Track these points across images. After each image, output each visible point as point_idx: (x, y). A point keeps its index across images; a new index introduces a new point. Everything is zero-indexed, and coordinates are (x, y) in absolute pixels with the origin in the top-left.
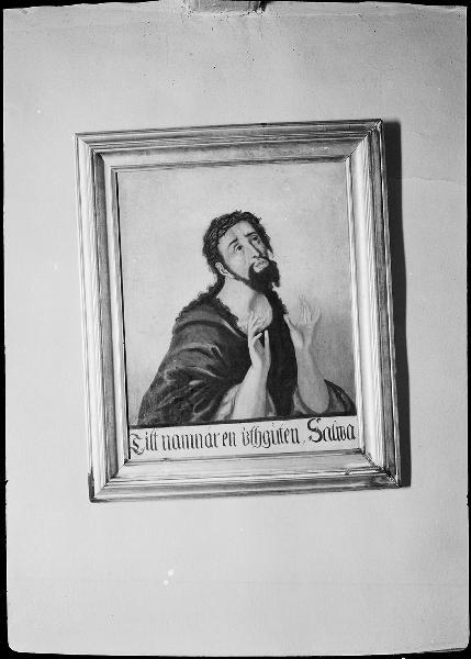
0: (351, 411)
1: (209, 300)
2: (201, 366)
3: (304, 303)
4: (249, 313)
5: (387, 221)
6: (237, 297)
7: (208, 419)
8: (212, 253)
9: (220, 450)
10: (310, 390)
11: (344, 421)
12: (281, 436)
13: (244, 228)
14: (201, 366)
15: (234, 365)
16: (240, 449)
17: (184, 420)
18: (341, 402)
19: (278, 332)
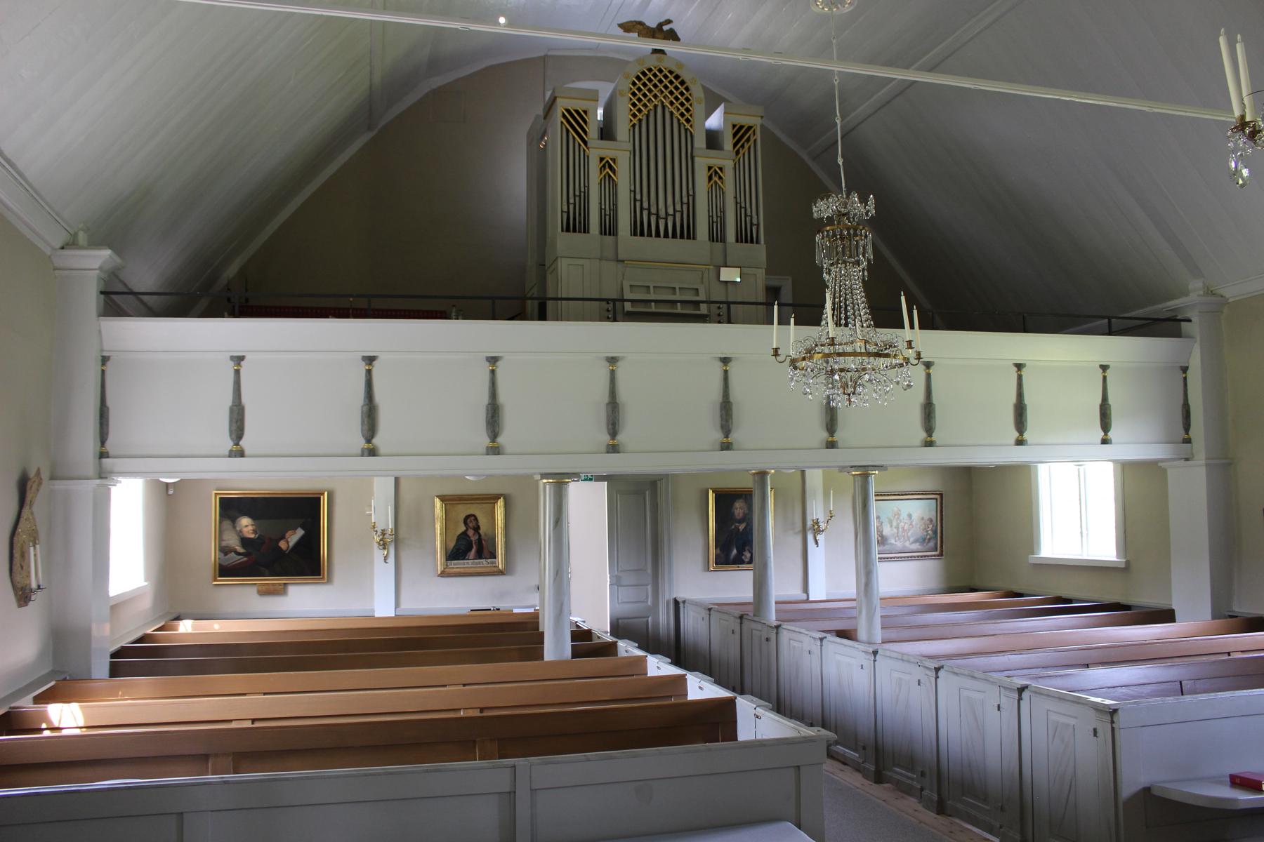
1: (465, 533)
6: (471, 533)
8: (465, 522)
10: (486, 552)
15: (470, 549)
18: (493, 556)
19: (480, 540)
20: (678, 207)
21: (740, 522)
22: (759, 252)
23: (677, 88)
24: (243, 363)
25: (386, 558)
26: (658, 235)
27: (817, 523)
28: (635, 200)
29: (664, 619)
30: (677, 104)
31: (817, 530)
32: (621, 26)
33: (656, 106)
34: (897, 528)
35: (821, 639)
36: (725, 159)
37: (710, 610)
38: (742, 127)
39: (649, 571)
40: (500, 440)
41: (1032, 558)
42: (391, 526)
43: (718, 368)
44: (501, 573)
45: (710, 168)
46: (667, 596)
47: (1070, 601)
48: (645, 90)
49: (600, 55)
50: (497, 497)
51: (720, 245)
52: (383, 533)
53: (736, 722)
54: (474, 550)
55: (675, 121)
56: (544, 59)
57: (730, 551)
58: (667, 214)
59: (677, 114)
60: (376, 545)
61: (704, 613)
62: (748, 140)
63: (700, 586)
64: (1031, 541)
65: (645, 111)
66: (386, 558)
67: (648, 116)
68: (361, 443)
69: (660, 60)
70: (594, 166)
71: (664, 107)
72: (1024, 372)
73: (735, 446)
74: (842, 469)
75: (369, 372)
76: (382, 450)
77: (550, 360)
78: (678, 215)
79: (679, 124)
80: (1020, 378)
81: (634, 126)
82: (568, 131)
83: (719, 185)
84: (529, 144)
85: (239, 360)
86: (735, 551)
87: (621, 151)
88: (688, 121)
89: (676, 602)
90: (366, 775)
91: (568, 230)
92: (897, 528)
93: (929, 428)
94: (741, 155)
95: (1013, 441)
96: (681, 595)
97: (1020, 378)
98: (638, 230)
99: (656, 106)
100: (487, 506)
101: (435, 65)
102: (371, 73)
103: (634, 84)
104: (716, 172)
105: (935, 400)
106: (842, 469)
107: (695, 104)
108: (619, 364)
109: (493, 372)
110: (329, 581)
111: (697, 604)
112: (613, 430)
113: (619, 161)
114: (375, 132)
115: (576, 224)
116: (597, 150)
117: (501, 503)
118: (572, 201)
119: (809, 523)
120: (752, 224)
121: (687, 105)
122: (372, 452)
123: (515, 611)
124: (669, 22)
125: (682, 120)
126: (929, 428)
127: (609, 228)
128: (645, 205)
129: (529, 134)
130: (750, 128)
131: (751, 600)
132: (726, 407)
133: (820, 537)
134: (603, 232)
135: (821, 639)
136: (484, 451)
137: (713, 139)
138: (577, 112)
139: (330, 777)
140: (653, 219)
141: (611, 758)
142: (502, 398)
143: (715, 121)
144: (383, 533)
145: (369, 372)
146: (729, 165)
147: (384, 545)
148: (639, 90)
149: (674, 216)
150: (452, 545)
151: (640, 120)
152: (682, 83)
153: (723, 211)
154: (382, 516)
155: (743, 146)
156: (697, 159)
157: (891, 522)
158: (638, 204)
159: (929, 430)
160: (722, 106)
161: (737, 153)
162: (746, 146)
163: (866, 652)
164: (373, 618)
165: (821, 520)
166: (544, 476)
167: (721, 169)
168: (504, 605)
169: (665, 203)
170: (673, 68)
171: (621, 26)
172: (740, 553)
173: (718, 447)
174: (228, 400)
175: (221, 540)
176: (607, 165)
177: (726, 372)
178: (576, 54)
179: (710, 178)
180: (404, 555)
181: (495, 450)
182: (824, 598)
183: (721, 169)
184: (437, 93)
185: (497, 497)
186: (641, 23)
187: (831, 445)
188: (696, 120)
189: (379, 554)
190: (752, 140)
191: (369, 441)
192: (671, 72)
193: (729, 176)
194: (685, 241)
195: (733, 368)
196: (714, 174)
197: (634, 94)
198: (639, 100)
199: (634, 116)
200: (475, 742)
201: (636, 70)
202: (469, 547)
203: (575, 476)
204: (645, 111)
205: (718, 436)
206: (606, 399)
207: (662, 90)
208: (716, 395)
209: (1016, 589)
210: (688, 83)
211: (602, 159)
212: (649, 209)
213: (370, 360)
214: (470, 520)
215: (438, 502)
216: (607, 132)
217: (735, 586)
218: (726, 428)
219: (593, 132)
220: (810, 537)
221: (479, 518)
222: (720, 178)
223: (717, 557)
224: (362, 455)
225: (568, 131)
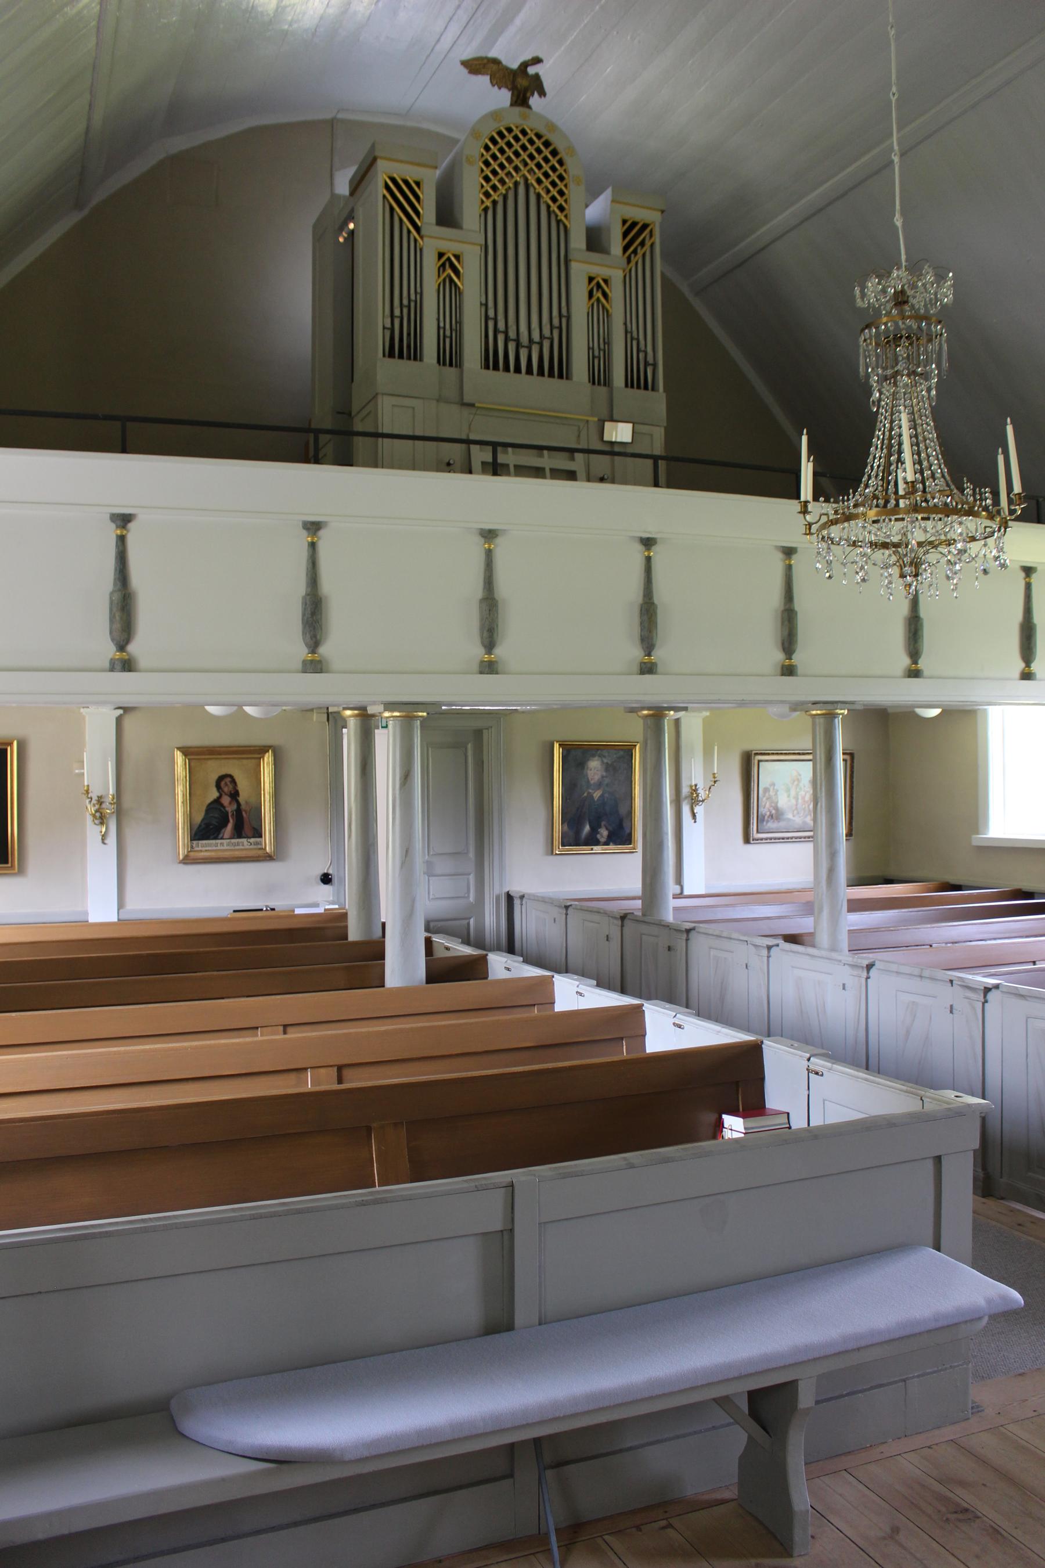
0: (261, 836)
1: (217, 801)
2: (214, 822)
3: (247, 803)
4: (231, 808)
6: (226, 800)
7: (216, 838)
8: (218, 786)
9: (219, 848)
10: (247, 828)
11: (258, 840)
12: (238, 844)
13: (228, 780)
14: (214, 822)
16: (225, 847)
17: (208, 838)
18: (258, 833)
19: (239, 811)
20: (546, 332)
22: (657, 402)
23: (546, 160)
25: (104, 838)
27: (696, 790)
28: (487, 318)
29: (492, 921)
30: (546, 183)
31: (694, 800)
32: (464, 63)
33: (516, 184)
34: (796, 798)
35: (769, 948)
36: (611, 267)
37: (567, 907)
38: (634, 224)
39: (472, 855)
40: (324, 650)
41: (977, 839)
42: (112, 791)
43: (636, 555)
44: (269, 858)
45: (591, 279)
46: (495, 890)
47: (1030, 895)
48: (502, 159)
49: (410, 124)
50: (262, 750)
51: (603, 390)
52: (100, 801)
53: (763, 1079)
54: (230, 826)
55: (543, 208)
56: (332, 123)
58: (531, 340)
59: (546, 198)
60: (89, 819)
61: (558, 913)
62: (642, 244)
63: (543, 874)
64: (974, 812)
65: (502, 190)
66: (104, 838)
67: (505, 198)
68: (110, 650)
69: (525, 117)
71: (527, 186)
72: (1034, 579)
73: (660, 668)
74: (797, 706)
75: (122, 540)
76: (143, 662)
77: (397, 528)
78: (546, 344)
79: (549, 212)
80: (1028, 587)
81: (486, 210)
82: (392, 209)
83: (604, 304)
84: (319, 237)
86: (587, 828)
87: (468, 243)
88: (561, 208)
89: (510, 898)
90: (254, 1218)
91: (391, 355)
92: (796, 798)
93: (914, 651)
94: (633, 264)
95: (1017, 675)
96: (516, 887)
97: (1028, 587)
98: (491, 361)
99: (516, 184)
100: (250, 763)
101: (176, 114)
102: (91, 105)
103: (487, 148)
104: (598, 285)
105: (922, 613)
106: (797, 706)
107: (572, 186)
108: (499, 540)
109: (313, 545)
110: (21, 871)
111: (544, 900)
113: (466, 258)
114: (86, 212)
115: (403, 347)
116: (435, 240)
117: (268, 758)
118: (397, 312)
119: (685, 791)
120: (646, 364)
121: (561, 185)
122: (128, 665)
123: (298, 911)
124: (537, 61)
125: (554, 207)
126: (914, 651)
127: (450, 356)
128: (501, 325)
129: (315, 227)
130: (645, 226)
131: (639, 893)
132: (648, 612)
133: (699, 810)
134: (440, 361)
135: (769, 948)
136: (300, 666)
137: (595, 240)
138: (406, 182)
139: (186, 1226)
140: (512, 347)
141: (667, 1160)
142: (328, 586)
143: (597, 210)
145: (122, 540)
146: (617, 276)
147: (101, 818)
148: (494, 157)
149: (541, 344)
150: (199, 818)
151: (495, 203)
152: (554, 153)
153: (608, 342)
154: (97, 773)
155: (635, 252)
156: (574, 266)
157: (788, 790)
158: (491, 324)
159: (915, 654)
160: (608, 193)
161: (629, 260)
162: (640, 252)
163: (854, 966)
165: (700, 786)
166: (389, 706)
167: (606, 281)
168: (280, 902)
169: (528, 325)
170: (543, 131)
171: (464, 63)
172: (594, 830)
173: (636, 668)
176: (448, 264)
177: (648, 559)
178: (377, 120)
179: (591, 295)
180: (129, 832)
181: (315, 666)
182: (702, 892)
183: (606, 281)
184: (176, 161)
185: (262, 750)
186: (496, 62)
187: (789, 671)
188: (573, 208)
189: (93, 831)
190: (648, 244)
191: (122, 647)
192: (539, 136)
193: (616, 292)
194: (555, 381)
196: (597, 287)
197: (487, 164)
198: (494, 172)
199: (487, 195)
200: (369, 1129)
201: (490, 129)
202: (224, 821)
204: (502, 190)
206: (479, 593)
208: (634, 592)
209: (953, 879)
210: (562, 154)
211: (441, 255)
212: (506, 333)
213: (124, 520)
215: (179, 757)
216: (447, 217)
217: (612, 875)
218: (648, 642)
219: (428, 210)
220: (686, 809)
222: (605, 295)
224: (112, 669)
225: (392, 209)
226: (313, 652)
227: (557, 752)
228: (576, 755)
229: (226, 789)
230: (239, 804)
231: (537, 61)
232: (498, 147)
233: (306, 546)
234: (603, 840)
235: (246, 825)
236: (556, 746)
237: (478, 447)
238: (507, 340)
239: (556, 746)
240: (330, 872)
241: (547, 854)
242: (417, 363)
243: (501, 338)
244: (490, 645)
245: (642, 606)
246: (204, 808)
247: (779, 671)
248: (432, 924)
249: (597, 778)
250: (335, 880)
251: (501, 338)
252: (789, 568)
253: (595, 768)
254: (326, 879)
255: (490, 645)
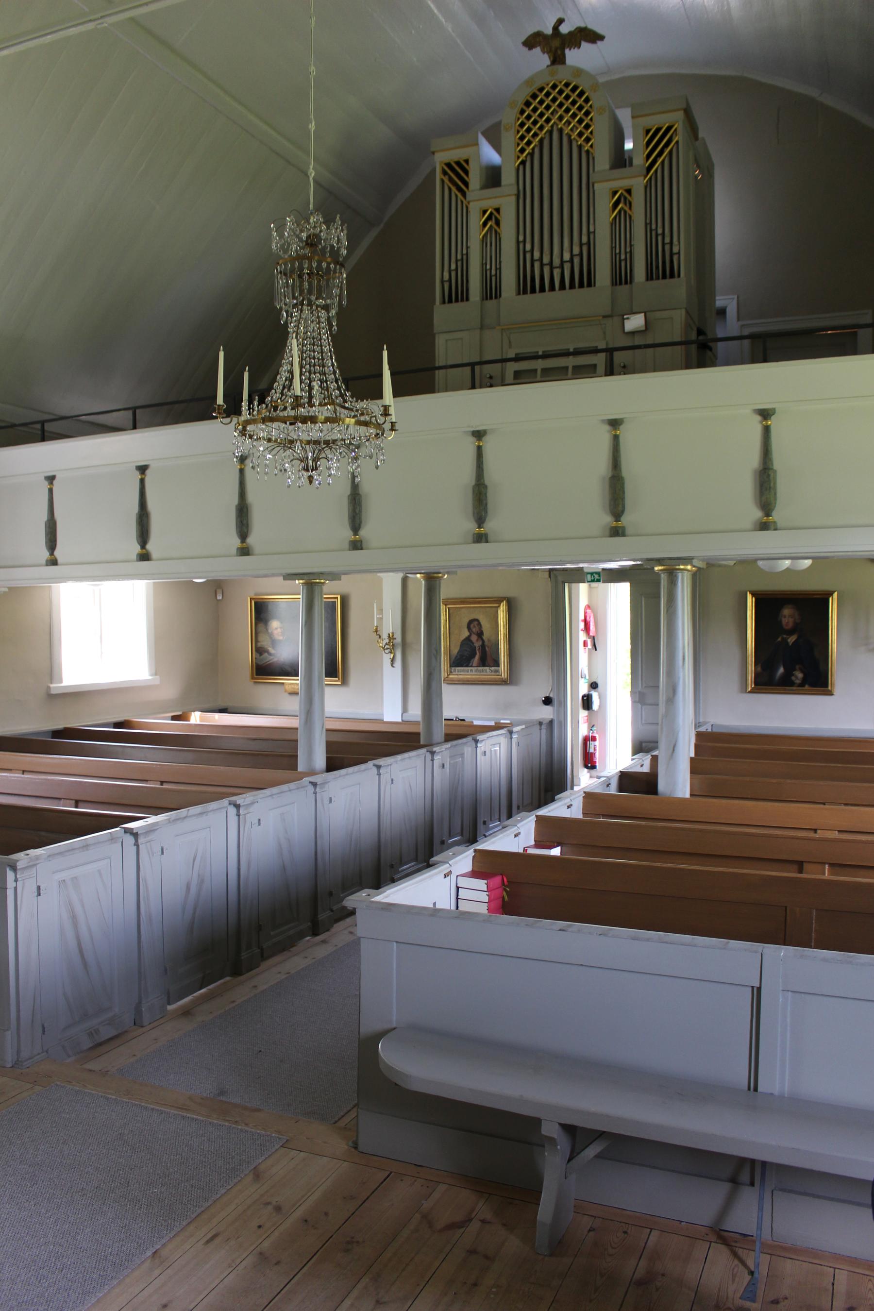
0: (498, 666)
1: (468, 639)
3: (489, 640)
4: (477, 644)
5: (10, 893)
6: (474, 638)
7: (467, 666)
11: (496, 668)
12: (483, 671)
13: (476, 623)
15: (473, 656)
18: (497, 664)
19: (483, 646)
21: (790, 632)
24: (55, 482)
25: (393, 661)
26: (552, 288)
43: (470, 444)
44: (504, 682)
50: (499, 601)
54: (477, 657)
57: (774, 669)
66: (393, 661)
70: (475, 221)
75: (142, 481)
76: (154, 555)
85: (51, 479)
86: (781, 670)
112: (356, 523)
124: (560, 21)
127: (492, 291)
140: (546, 270)
142: (251, 497)
144: (391, 638)
145: (142, 481)
150: (455, 651)
152: (534, 96)
164: (381, 721)
174: (45, 517)
175: (257, 641)
176: (493, 218)
177: (479, 448)
185: (499, 601)
189: (387, 658)
191: (52, 554)
193: (638, 199)
195: (490, 445)
196: (622, 199)
203: (578, 576)
205: (471, 526)
207: (555, 108)
208: (602, 466)
214: (474, 624)
221: (481, 621)
223: (757, 676)
224: (47, 565)
226: (479, 527)
227: (750, 601)
228: (769, 605)
229: (474, 630)
230: (483, 641)
231: (560, 21)
232: (564, 101)
233: (138, 481)
234: (798, 682)
235: (488, 658)
236: (749, 597)
237: (600, 347)
238: (542, 265)
239: (749, 597)
240: (551, 696)
241: (742, 692)
242: (465, 303)
243: (537, 265)
244: (480, 520)
245: (474, 487)
246: (459, 644)
247: (608, 533)
248: (644, 745)
249: (791, 625)
250: (555, 702)
251: (537, 265)
252: (616, 438)
253: (788, 616)
254: (548, 701)
255: (480, 520)
